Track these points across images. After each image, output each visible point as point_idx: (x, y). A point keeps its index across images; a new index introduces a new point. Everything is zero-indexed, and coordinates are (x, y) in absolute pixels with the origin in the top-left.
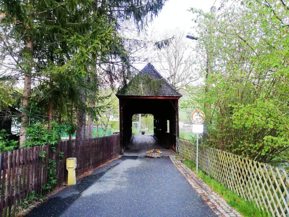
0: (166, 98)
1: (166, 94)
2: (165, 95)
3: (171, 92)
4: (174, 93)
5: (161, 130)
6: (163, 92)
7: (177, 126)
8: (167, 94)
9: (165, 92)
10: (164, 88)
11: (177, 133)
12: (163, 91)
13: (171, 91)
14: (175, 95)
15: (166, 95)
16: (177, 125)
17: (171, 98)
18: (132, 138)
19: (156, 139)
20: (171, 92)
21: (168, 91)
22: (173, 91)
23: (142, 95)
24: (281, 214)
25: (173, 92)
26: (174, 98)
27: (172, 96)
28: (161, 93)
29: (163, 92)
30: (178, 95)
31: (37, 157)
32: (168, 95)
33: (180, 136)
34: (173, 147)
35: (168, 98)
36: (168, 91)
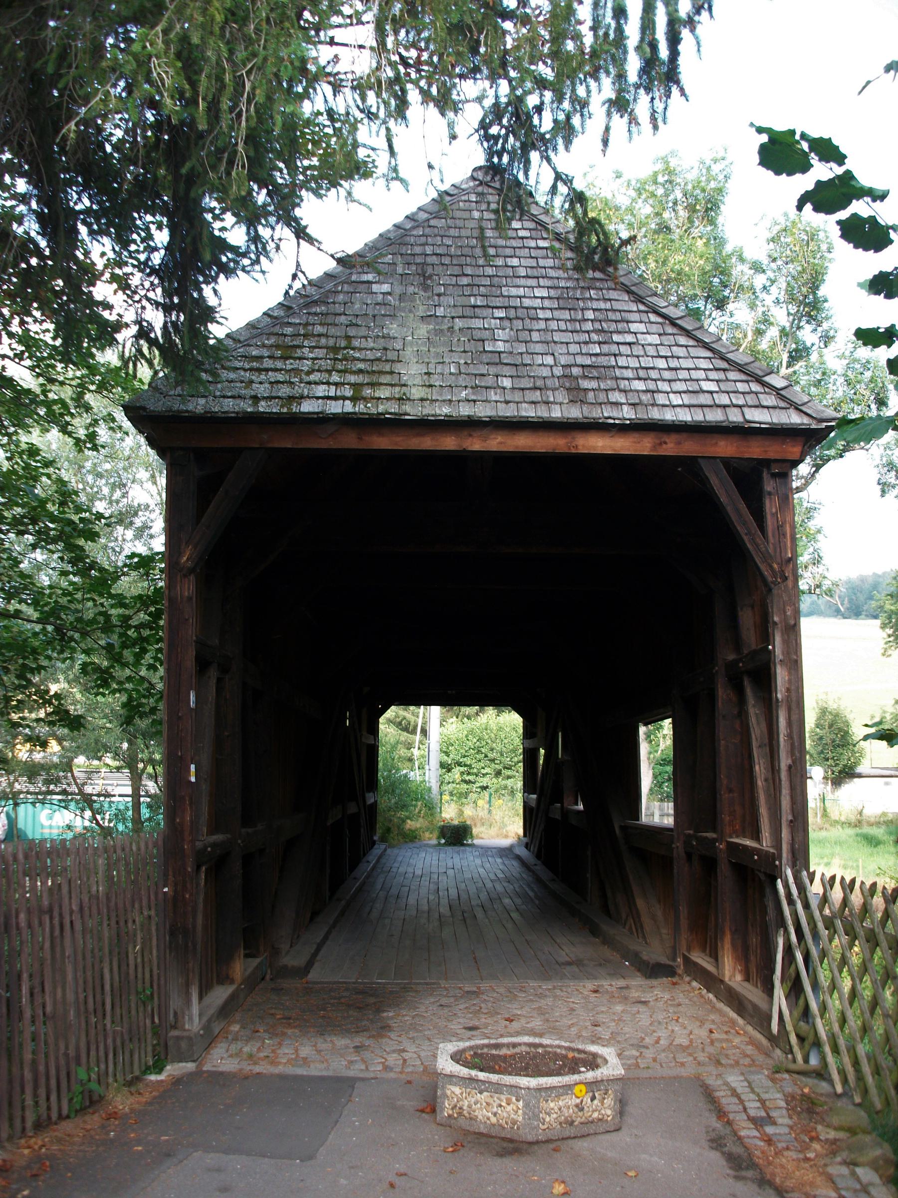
0: (671, 447)
1: (661, 399)
2: (655, 414)
3: (712, 386)
4: (751, 400)
5: (166, 137)
6: (639, 385)
7: (792, 752)
8: (676, 400)
9: (651, 385)
10: (637, 350)
11: (471, 1079)
12: (629, 374)
13: (721, 375)
14: (759, 417)
15: (669, 416)
16: (790, 736)
17: (725, 448)
18: (364, 868)
19: (538, 880)
20: (712, 386)
21: (683, 374)
22: (732, 375)
23: (413, 411)
24: (797, 998)
25: (741, 387)
26: (755, 450)
27: (735, 417)
28: (615, 396)
29: (639, 385)
30: (795, 419)
31: (322, 934)
32: (685, 416)
33: (816, 864)
34: (715, 956)
35: (689, 447)
36: (683, 374)
